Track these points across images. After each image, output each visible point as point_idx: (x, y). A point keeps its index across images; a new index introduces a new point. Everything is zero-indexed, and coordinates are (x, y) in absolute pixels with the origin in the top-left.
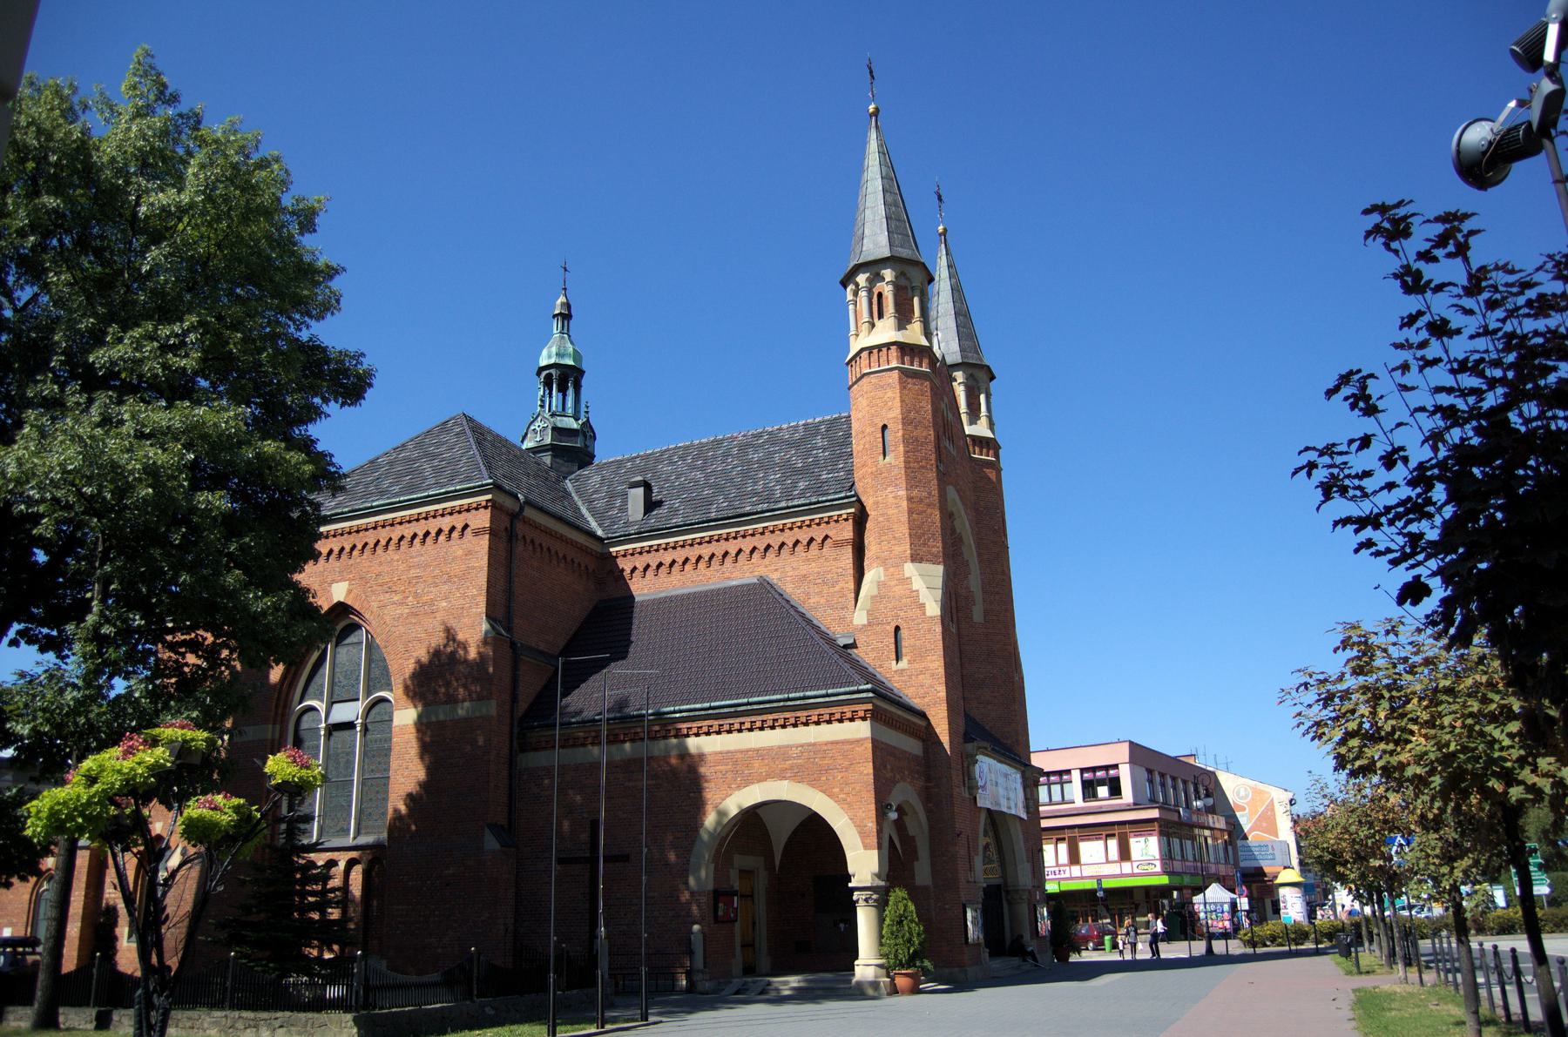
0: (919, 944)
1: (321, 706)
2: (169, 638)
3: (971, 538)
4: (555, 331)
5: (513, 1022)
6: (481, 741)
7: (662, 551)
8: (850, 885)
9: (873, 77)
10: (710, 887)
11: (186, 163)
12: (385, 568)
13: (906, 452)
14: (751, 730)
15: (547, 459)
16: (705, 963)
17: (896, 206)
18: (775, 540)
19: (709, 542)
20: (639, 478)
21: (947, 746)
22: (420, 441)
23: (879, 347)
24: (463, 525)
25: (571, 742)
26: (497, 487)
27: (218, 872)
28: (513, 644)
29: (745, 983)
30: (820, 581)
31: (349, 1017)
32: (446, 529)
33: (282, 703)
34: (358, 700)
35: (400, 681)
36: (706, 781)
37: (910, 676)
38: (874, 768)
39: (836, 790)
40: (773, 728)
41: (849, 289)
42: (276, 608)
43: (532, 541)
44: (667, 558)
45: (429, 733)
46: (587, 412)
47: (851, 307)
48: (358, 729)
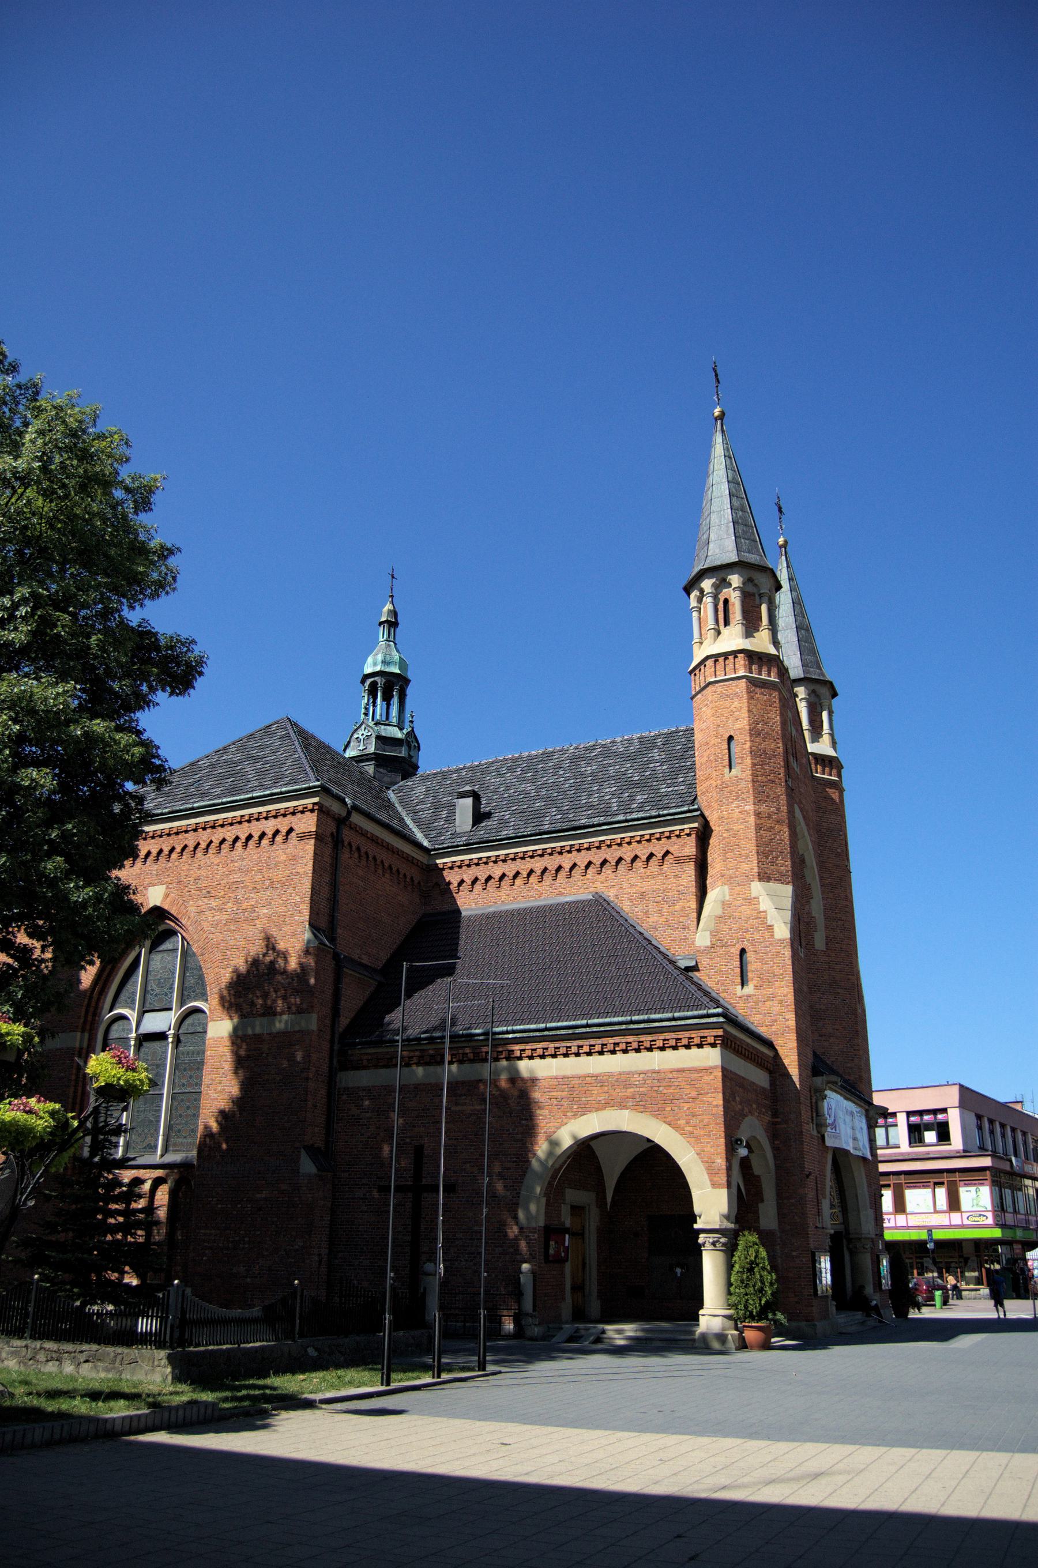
0: (772, 1294)
1: (132, 1015)
3: (814, 859)
4: (381, 639)
5: (338, 1366)
6: (299, 1056)
7: (491, 864)
8: (696, 1226)
9: (718, 381)
11: (21, 434)
12: (204, 872)
13: (754, 765)
14: (589, 1054)
15: (370, 768)
16: (534, 1306)
17: (743, 510)
18: (612, 855)
19: (542, 856)
20: (468, 788)
21: (796, 1079)
22: (241, 744)
23: (726, 655)
24: (287, 828)
26: (325, 790)
27: (29, 1184)
28: (336, 956)
29: (577, 1330)
31: (162, 1354)
32: (270, 833)
33: (92, 1009)
34: (170, 1009)
35: (215, 990)
36: (539, 1108)
37: (757, 1003)
38: (725, 1099)
39: (682, 1122)
40: (613, 1052)
41: (692, 596)
42: (98, 899)
43: (358, 849)
44: (497, 871)
45: (244, 1046)
46: (412, 722)
47: (695, 614)
48: (170, 1040)
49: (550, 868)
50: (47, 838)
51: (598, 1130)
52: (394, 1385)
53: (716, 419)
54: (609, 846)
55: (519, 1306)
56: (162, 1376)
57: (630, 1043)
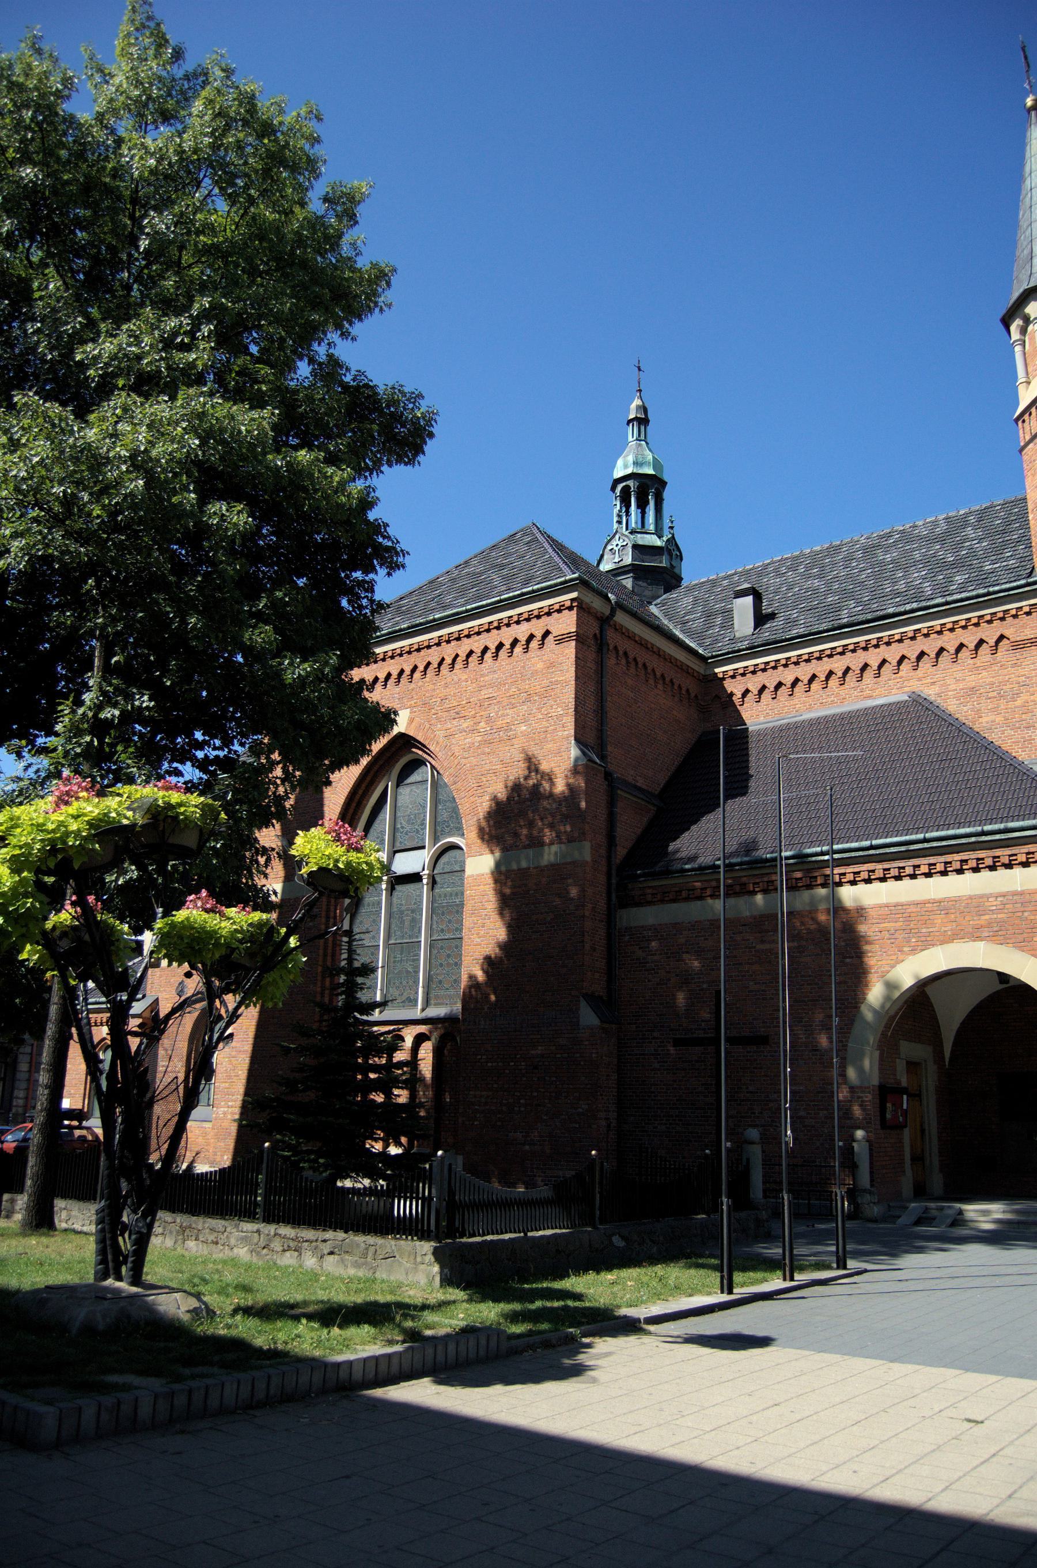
2: (200, 754)
4: (630, 439)
6: (574, 892)
7: (781, 668)
10: (875, 1081)
12: (451, 690)
14: (928, 875)
15: (628, 582)
16: (872, 1181)
19: (842, 653)
20: (746, 586)
22: (483, 556)
24: (542, 632)
25: (684, 894)
28: (608, 775)
29: (927, 1209)
30: (995, 694)
31: (426, 1247)
34: (423, 847)
36: (868, 943)
40: (960, 871)
41: (1013, 328)
43: (625, 654)
44: (788, 676)
45: (509, 883)
46: (671, 528)
47: (1018, 349)
48: (425, 881)
49: (853, 667)
50: (254, 609)
51: (944, 967)
52: (739, 1292)
53: (1029, 110)
54: (990, 622)
55: (854, 1179)
56: (427, 1277)
57: (983, 859)
